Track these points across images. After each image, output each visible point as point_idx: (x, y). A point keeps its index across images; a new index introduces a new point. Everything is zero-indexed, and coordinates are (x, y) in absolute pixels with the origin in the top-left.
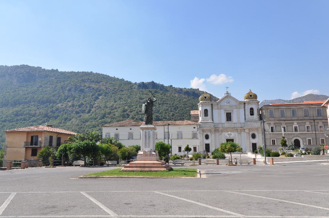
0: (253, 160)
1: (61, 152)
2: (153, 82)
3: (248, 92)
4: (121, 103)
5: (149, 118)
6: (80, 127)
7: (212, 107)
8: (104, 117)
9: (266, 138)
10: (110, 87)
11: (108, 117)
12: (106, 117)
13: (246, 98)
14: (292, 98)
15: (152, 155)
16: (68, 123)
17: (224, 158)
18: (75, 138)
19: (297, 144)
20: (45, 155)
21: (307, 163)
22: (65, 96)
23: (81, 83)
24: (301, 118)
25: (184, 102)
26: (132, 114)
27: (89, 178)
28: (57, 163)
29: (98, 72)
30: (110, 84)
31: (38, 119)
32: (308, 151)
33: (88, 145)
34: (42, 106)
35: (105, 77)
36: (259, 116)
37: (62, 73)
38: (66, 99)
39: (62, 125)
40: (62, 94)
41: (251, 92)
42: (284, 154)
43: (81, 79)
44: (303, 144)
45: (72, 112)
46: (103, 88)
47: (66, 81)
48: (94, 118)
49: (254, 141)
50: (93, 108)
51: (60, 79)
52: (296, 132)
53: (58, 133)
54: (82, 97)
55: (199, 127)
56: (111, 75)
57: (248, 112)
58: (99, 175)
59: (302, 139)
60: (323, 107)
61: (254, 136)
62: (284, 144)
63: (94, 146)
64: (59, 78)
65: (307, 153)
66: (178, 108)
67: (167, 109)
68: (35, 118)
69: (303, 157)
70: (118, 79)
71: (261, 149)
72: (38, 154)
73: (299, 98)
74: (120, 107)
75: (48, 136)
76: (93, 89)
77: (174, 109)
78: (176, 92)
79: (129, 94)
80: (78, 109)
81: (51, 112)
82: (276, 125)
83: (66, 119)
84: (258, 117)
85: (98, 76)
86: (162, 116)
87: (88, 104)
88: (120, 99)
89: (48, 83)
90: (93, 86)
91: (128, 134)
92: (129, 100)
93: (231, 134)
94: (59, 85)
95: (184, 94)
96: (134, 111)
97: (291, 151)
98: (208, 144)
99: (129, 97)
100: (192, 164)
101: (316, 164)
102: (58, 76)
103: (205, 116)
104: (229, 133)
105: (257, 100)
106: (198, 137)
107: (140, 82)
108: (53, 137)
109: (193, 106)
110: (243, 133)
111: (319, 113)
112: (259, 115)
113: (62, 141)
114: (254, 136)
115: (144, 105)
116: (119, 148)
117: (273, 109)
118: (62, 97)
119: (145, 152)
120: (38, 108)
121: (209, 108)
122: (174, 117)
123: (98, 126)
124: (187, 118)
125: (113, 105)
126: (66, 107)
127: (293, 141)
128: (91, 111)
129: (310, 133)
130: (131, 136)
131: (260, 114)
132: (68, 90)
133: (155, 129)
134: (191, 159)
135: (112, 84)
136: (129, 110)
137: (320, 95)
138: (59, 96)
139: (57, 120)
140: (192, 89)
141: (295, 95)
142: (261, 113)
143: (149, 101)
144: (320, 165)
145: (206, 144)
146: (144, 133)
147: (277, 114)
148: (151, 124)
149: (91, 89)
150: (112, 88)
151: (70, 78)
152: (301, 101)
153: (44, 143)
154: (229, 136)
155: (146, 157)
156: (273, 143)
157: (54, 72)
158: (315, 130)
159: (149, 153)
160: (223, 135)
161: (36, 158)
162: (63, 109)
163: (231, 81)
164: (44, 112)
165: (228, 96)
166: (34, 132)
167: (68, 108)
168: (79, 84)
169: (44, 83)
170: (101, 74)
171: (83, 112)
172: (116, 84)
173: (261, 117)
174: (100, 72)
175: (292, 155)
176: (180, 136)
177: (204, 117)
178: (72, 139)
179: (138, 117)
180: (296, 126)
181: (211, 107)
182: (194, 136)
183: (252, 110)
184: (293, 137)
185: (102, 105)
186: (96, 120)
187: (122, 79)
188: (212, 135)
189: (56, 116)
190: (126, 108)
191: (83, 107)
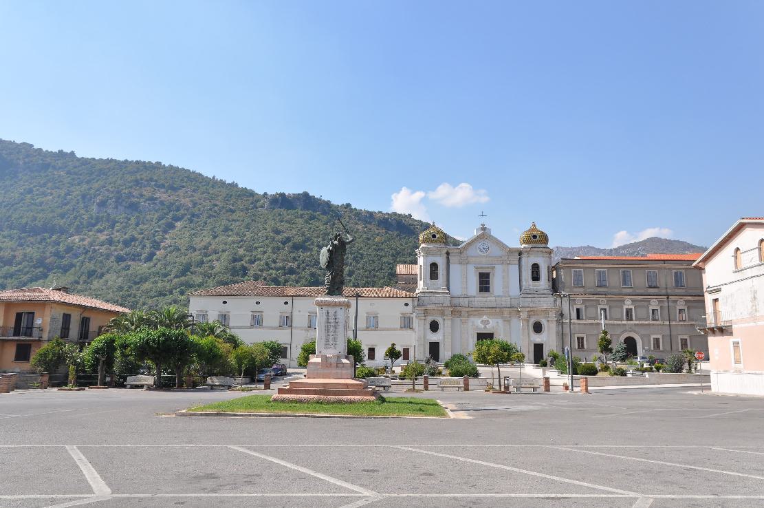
0: (542, 382)
1: (98, 354)
2: (306, 195)
4: (231, 239)
5: (338, 280)
6: (127, 293)
7: (448, 258)
8: (186, 270)
10: (204, 201)
12: (192, 273)
14: (615, 245)
15: (342, 365)
16: (95, 282)
17: (476, 375)
18: (127, 320)
19: (630, 348)
20: (51, 360)
21: (658, 390)
22: (91, 218)
23: (131, 187)
24: (642, 291)
25: (377, 244)
26: (254, 269)
27: (201, 415)
28: (85, 380)
29: (175, 164)
30: (203, 193)
31: (18, 271)
32: (656, 365)
33: (168, 338)
34: (32, 239)
36: (551, 284)
37: (85, 162)
38: (94, 225)
39: (79, 287)
40: (82, 212)
41: (534, 228)
42: (606, 368)
43: (133, 178)
44: (643, 349)
45: (108, 256)
46: (186, 202)
47: (95, 181)
49: (538, 339)
50: (159, 249)
51: (79, 176)
53: (85, 308)
54: (133, 220)
55: (416, 303)
56: (208, 173)
57: (527, 274)
58: (226, 409)
60: (696, 267)
61: (538, 328)
62: (606, 347)
63: (182, 341)
65: (654, 369)
66: (362, 258)
68: (13, 269)
69: (647, 376)
70: (222, 183)
71: (555, 357)
72: (31, 357)
73: (631, 246)
75: (59, 313)
76: (162, 203)
77: (354, 259)
78: (359, 220)
79: (247, 220)
81: (55, 256)
83: (91, 274)
84: (549, 286)
85: (174, 173)
88: (227, 229)
89: (49, 185)
90: (162, 195)
91: (251, 313)
93: (488, 322)
94: (77, 191)
95: (379, 226)
96: (259, 259)
97: (618, 362)
98: (437, 344)
103: (432, 278)
104: (485, 318)
105: (548, 246)
107: (274, 193)
110: (514, 321)
111: (678, 279)
112: (551, 279)
113: (93, 327)
114: (538, 328)
115: (324, 250)
116: (235, 347)
118: (83, 219)
119: (325, 358)
120: (21, 245)
121: (441, 261)
123: (171, 293)
124: (382, 281)
125: (210, 244)
126: (91, 244)
127: (622, 339)
128: (155, 257)
129: (658, 325)
130: (257, 321)
131: (553, 279)
132: (98, 204)
134: (402, 378)
135: (209, 193)
136: (247, 258)
137: (674, 241)
138: (75, 218)
139: (67, 274)
140: (395, 214)
141: (621, 239)
143: (336, 242)
147: (590, 280)
148: (340, 294)
150: (208, 203)
151: (106, 175)
152: (635, 252)
153: (49, 333)
154: (483, 326)
155: (326, 371)
156: (579, 346)
157: (64, 157)
158: (669, 317)
159: (334, 361)
161: (25, 366)
162: (84, 248)
163: (484, 199)
164: (36, 255)
165: (484, 234)
166: (24, 303)
167: (97, 248)
169: (39, 183)
171: (135, 257)
173: (555, 286)
175: (623, 373)
176: (373, 324)
178: (117, 321)
179: (268, 275)
182: (407, 323)
183: (535, 268)
185: (183, 243)
186: (166, 279)
187: (234, 182)
188: (446, 322)
189: (65, 266)
190: (241, 252)
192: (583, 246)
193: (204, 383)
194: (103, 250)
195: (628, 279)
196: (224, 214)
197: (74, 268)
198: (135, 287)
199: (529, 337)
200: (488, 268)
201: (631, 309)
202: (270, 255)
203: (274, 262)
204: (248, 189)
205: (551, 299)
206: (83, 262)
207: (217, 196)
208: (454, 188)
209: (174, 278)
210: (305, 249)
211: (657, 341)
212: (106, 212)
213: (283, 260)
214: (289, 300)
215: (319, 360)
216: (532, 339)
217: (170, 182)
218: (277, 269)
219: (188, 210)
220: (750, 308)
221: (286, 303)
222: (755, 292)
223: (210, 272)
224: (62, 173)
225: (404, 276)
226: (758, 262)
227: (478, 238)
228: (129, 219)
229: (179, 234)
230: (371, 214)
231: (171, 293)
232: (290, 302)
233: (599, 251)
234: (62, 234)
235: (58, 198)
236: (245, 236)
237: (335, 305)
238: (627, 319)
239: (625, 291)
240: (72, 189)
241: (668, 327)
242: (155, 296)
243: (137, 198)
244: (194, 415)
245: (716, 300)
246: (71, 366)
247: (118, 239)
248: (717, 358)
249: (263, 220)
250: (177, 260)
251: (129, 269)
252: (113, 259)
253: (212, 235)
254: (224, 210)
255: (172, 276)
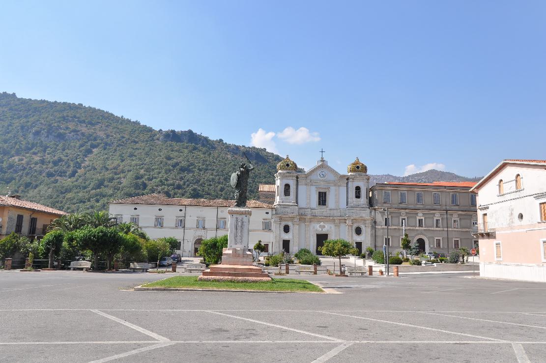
2: (190, 132)
3: (353, 162)
7: (297, 181)
8: (100, 184)
9: (377, 234)
11: (107, 186)
13: (350, 171)
14: (406, 174)
18: (66, 220)
20: (9, 249)
22: (28, 143)
23: (59, 122)
24: (465, 208)
27: (153, 290)
29: (93, 106)
32: (439, 258)
33: (105, 234)
35: (106, 115)
37: (24, 102)
38: (31, 149)
42: (407, 260)
44: (430, 247)
45: (41, 173)
46: (101, 134)
47: (31, 116)
48: (82, 186)
50: (80, 169)
52: (421, 228)
53: (34, 211)
56: (117, 113)
57: (352, 193)
59: (429, 238)
60: (472, 192)
61: (358, 231)
64: (16, 110)
65: (439, 261)
67: (213, 179)
70: (129, 121)
73: (417, 175)
74: (131, 171)
75: (15, 214)
76: (83, 134)
78: (228, 151)
80: (52, 168)
82: (409, 215)
83: (27, 185)
84: (367, 202)
85: (93, 112)
86: (203, 190)
87: (72, 161)
88: (131, 155)
90: (84, 129)
92: (148, 160)
93: (324, 227)
94: (17, 123)
95: (242, 156)
96: (155, 178)
99: (147, 154)
100: (277, 272)
101: (457, 277)
102: (16, 105)
104: (322, 224)
106: (273, 228)
108: (24, 217)
109: (256, 176)
110: (342, 225)
113: (39, 225)
114: (358, 231)
117: (389, 190)
118: (22, 144)
119: (235, 251)
122: (223, 193)
123: (89, 201)
126: (28, 164)
127: (415, 240)
128: (77, 174)
130: (159, 223)
133: (250, 213)
136: (146, 177)
137: (446, 172)
138: (16, 143)
140: (254, 148)
141: (409, 170)
142: (371, 196)
144: (463, 278)
145: (284, 241)
146: (234, 219)
147: (395, 198)
149: (78, 135)
153: (7, 228)
159: (241, 253)
160: (311, 228)
163: (317, 139)
165: (323, 165)
168: (56, 124)
170: (99, 110)
171: (62, 174)
172: (125, 131)
173: (371, 203)
174: (97, 106)
175: (419, 264)
177: (284, 197)
180: (422, 218)
181: (295, 182)
182: (267, 227)
183: (358, 189)
184: (416, 235)
185: (98, 164)
186: (85, 190)
187: (137, 121)
190: (142, 172)
191: (61, 165)
192: (385, 174)
193: (128, 266)
194: (37, 167)
195: (421, 198)
196: (129, 144)
197: (14, 181)
198: (61, 196)
199: (352, 236)
200: (325, 188)
201: (422, 219)
202: (163, 175)
203: (167, 180)
204: (148, 126)
205: (368, 210)
206: (21, 176)
207: (125, 131)
208: (296, 130)
209: (92, 189)
210: (189, 171)
211: (438, 241)
212: (40, 139)
213: (173, 179)
214: (183, 208)
215: (230, 252)
216: (354, 239)
217: (89, 119)
218: (168, 185)
219: (102, 140)
220: (508, 220)
221: (181, 210)
222: (513, 210)
223: (119, 186)
224: (6, 109)
225: (269, 193)
226: (515, 190)
227: (319, 167)
228: (58, 146)
229: (96, 157)
230: (237, 148)
231: (89, 201)
232: (184, 209)
233: (395, 178)
234: (5, 155)
235: (3, 127)
236: (145, 160)
237: (242, 213)
238: (420, 226)
239: (418, 206)
240: (13, 121)
241: (446, 232)
242: (77, 203)
243: (64, 130)
244: (148, 290)
245: (485, 215)
246: (30, 253)
247: (49, 160)
248: (484, 254)
249: (158, 149)
250: (93, 176)
251: (57, 182)
252: (44, 174)
253: (121, 159)
254: (130, 141)
255: (90, 189)
